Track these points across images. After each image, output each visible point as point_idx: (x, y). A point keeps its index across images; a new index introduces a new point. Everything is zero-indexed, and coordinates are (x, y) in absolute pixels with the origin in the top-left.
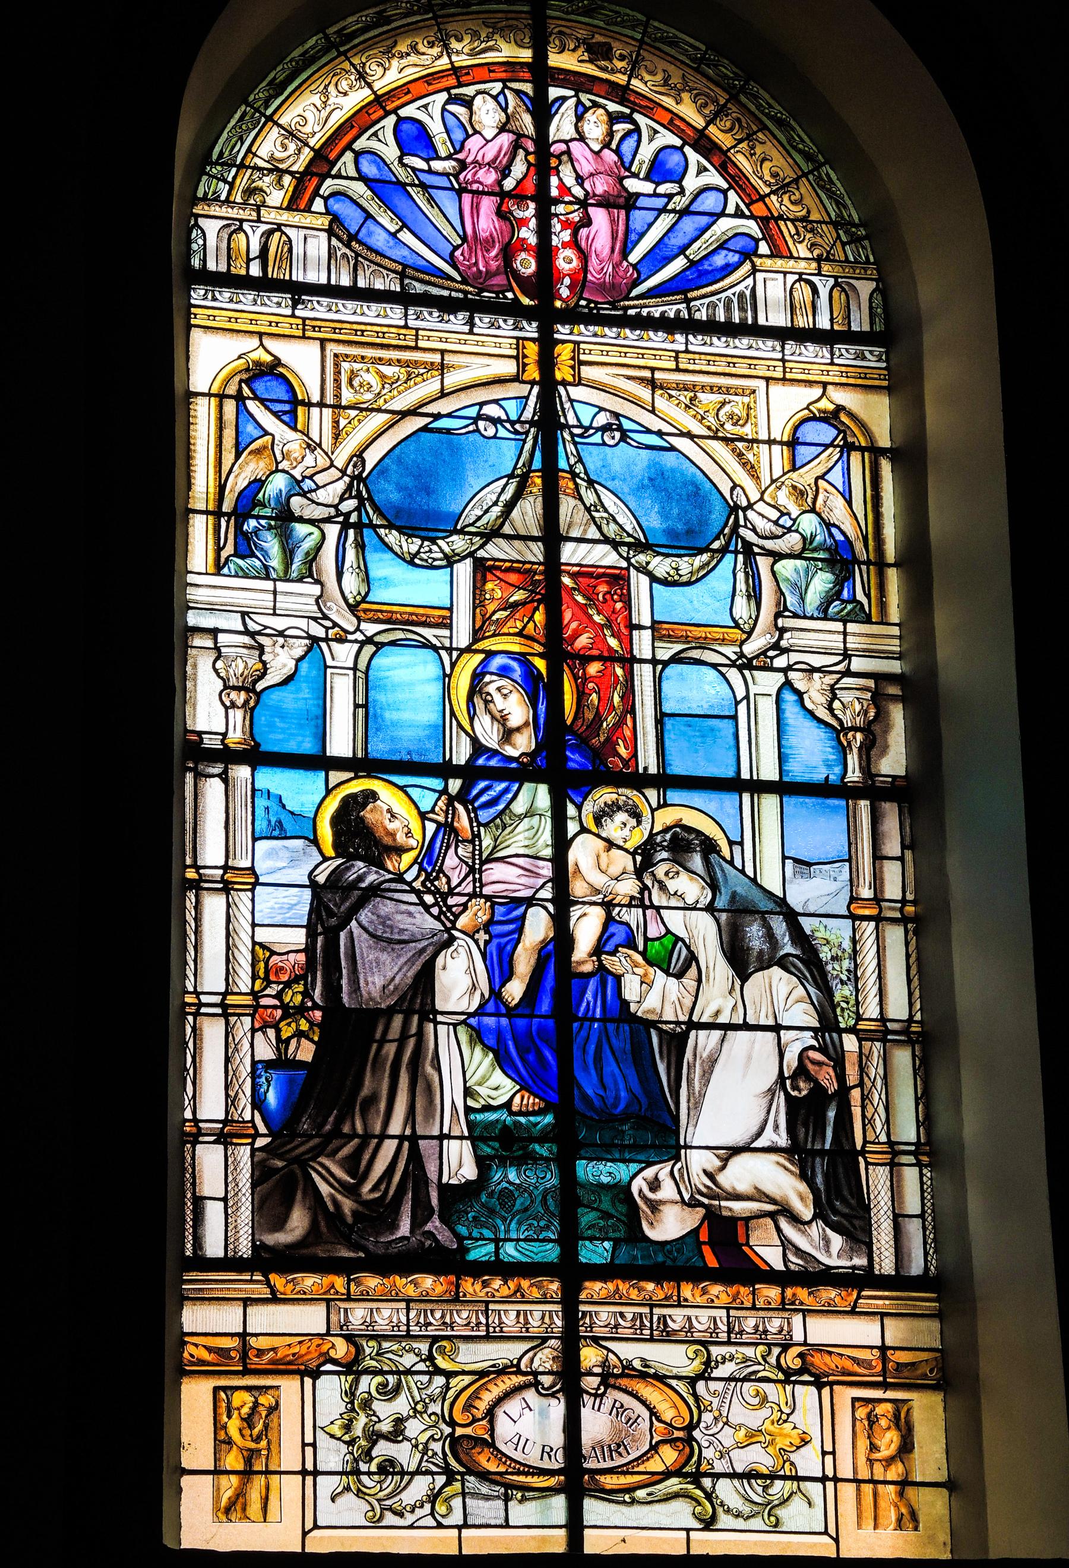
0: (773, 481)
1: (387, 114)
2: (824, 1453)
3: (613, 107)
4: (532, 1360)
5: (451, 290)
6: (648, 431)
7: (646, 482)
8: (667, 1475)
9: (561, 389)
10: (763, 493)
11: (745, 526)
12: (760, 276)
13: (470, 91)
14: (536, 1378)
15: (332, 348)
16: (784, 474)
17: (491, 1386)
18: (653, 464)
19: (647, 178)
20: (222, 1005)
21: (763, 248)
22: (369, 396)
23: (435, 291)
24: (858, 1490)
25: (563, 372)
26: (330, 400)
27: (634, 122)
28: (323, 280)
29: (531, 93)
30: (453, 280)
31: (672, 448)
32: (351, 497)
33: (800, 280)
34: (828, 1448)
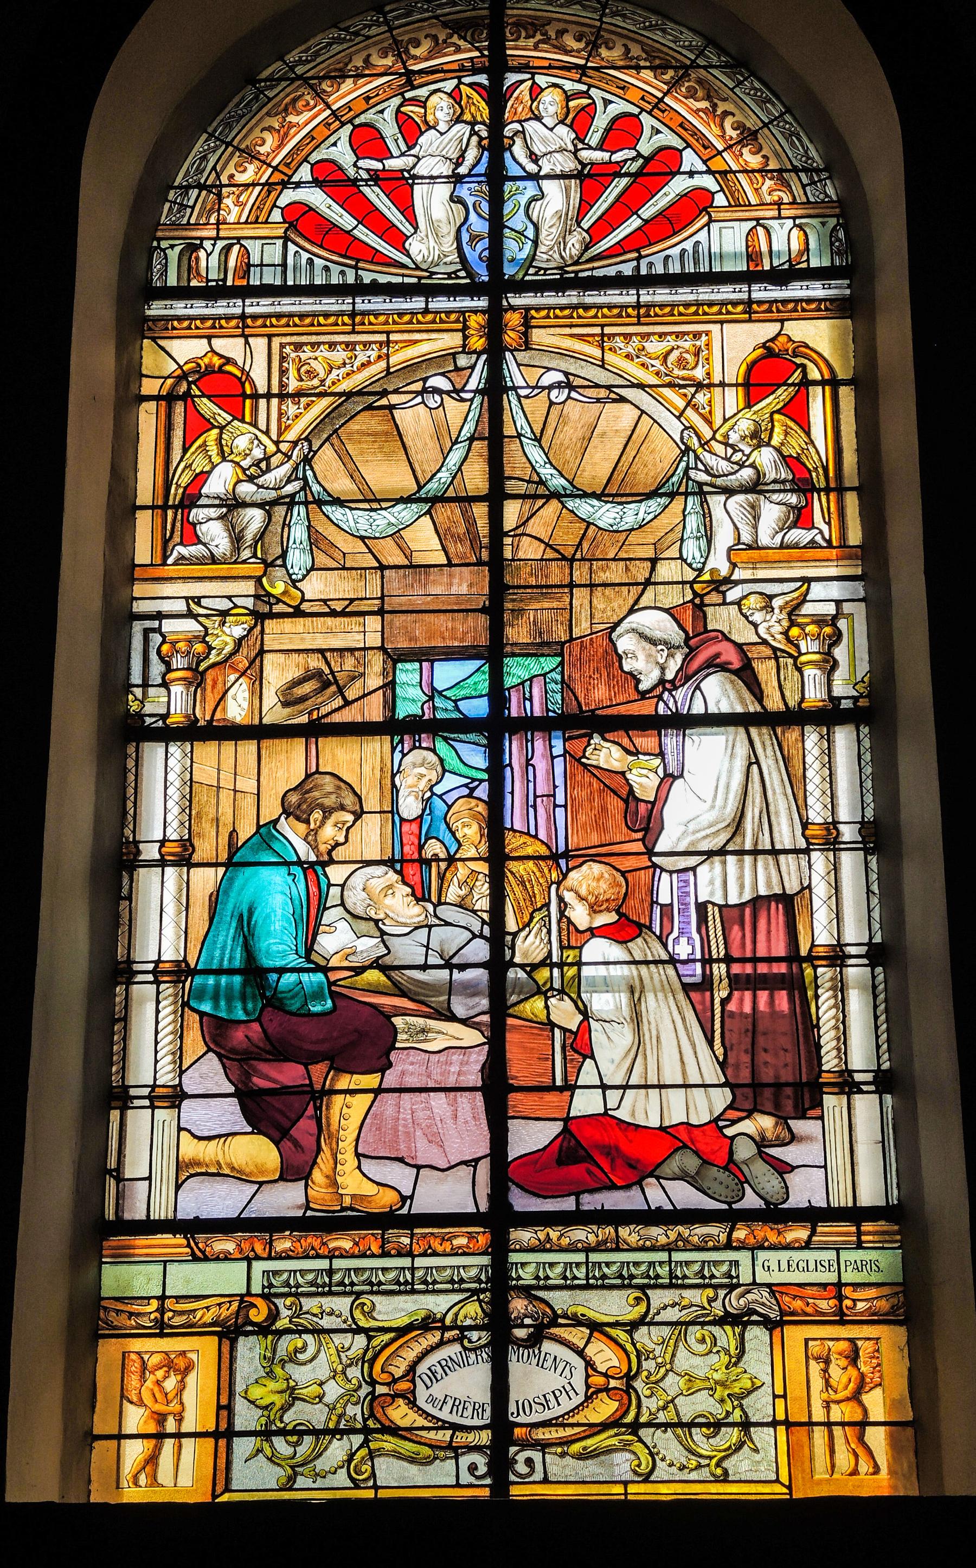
0: (725, 420)
1: (343, 124)
2: (775, 1396)
3: (568, 85)
4: (457, 1315)
5: (403, 275)
6: (597, 386)
7: (292, 1383)
8: (604, 1426)
9: (508, 354)
10: (715, 432)
11: (696, 468)
12: (715, 227)
13: (423, 92)
14: (462, 1333)
15: (276, 342)
16: (739, 412)
17: (414, 1345)
18: (384, 1067)
19: (600, 147)
20: (154, 972)
21: (720, 200)
22: (316, 382)
23: (383, 279)
24: (810, 1417)
25: (510, 337)
26: (275, 390)
27: (590, 97)
28: (278, 282)
29: (486, 82)
30: (404, 266)
31: (622, 400)
32: (297, 479)
33: (758, 224)
34: (779, 1391)
